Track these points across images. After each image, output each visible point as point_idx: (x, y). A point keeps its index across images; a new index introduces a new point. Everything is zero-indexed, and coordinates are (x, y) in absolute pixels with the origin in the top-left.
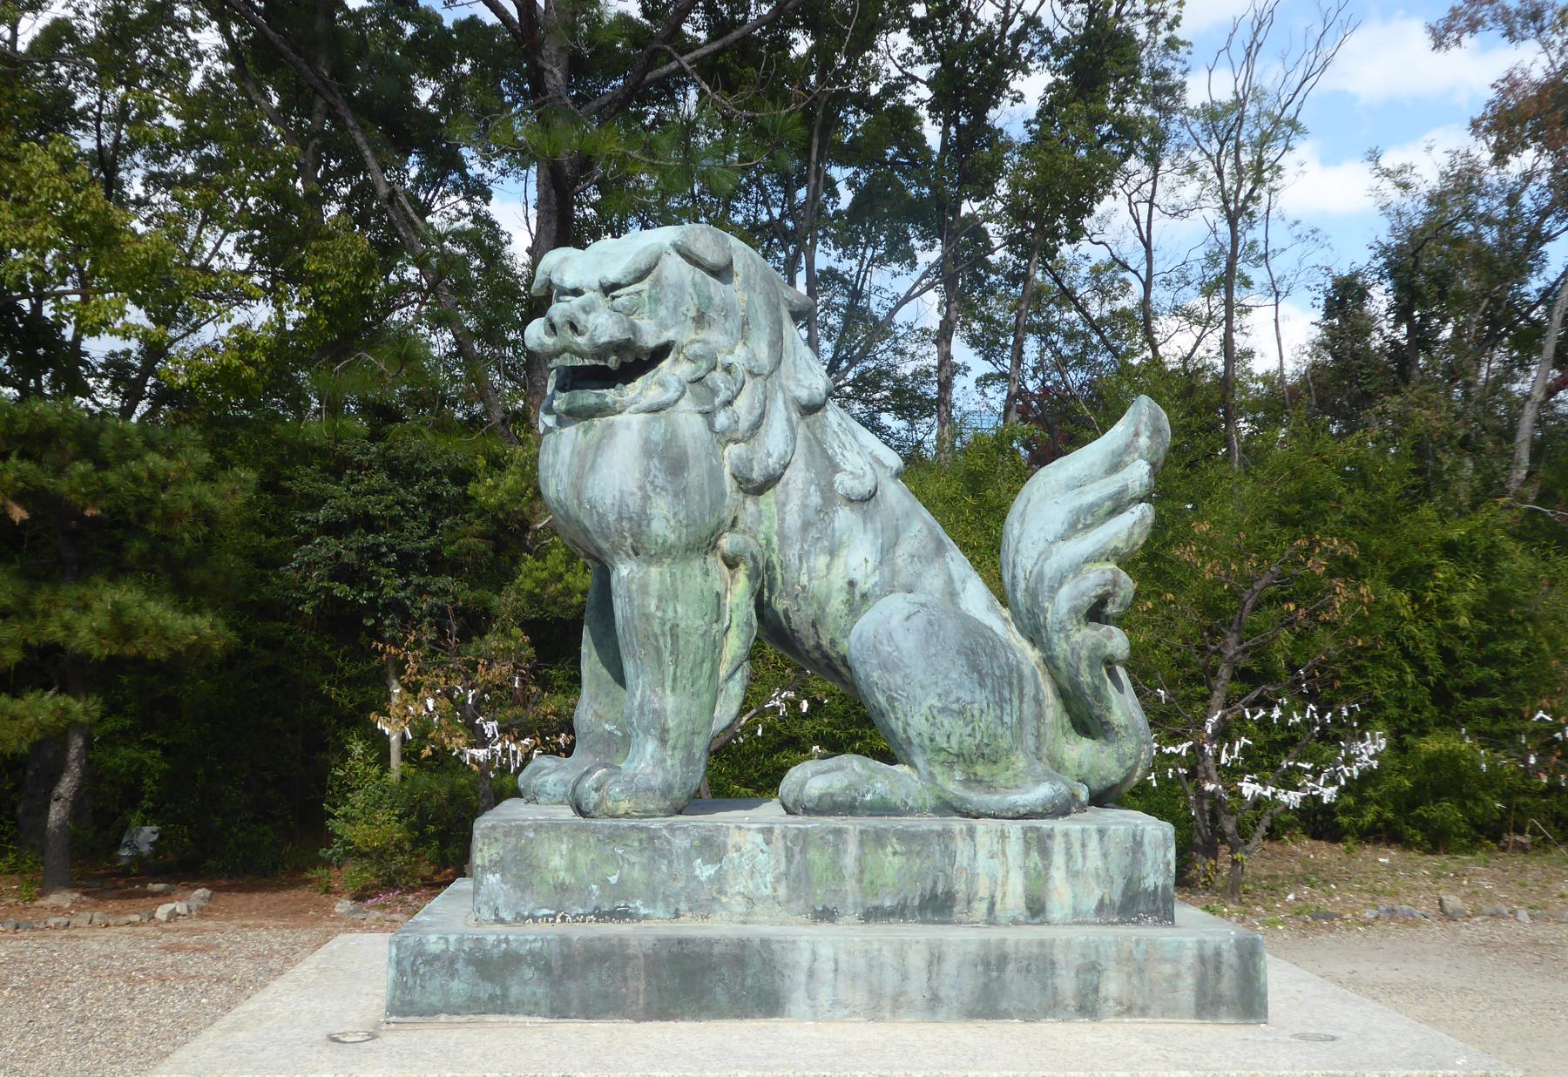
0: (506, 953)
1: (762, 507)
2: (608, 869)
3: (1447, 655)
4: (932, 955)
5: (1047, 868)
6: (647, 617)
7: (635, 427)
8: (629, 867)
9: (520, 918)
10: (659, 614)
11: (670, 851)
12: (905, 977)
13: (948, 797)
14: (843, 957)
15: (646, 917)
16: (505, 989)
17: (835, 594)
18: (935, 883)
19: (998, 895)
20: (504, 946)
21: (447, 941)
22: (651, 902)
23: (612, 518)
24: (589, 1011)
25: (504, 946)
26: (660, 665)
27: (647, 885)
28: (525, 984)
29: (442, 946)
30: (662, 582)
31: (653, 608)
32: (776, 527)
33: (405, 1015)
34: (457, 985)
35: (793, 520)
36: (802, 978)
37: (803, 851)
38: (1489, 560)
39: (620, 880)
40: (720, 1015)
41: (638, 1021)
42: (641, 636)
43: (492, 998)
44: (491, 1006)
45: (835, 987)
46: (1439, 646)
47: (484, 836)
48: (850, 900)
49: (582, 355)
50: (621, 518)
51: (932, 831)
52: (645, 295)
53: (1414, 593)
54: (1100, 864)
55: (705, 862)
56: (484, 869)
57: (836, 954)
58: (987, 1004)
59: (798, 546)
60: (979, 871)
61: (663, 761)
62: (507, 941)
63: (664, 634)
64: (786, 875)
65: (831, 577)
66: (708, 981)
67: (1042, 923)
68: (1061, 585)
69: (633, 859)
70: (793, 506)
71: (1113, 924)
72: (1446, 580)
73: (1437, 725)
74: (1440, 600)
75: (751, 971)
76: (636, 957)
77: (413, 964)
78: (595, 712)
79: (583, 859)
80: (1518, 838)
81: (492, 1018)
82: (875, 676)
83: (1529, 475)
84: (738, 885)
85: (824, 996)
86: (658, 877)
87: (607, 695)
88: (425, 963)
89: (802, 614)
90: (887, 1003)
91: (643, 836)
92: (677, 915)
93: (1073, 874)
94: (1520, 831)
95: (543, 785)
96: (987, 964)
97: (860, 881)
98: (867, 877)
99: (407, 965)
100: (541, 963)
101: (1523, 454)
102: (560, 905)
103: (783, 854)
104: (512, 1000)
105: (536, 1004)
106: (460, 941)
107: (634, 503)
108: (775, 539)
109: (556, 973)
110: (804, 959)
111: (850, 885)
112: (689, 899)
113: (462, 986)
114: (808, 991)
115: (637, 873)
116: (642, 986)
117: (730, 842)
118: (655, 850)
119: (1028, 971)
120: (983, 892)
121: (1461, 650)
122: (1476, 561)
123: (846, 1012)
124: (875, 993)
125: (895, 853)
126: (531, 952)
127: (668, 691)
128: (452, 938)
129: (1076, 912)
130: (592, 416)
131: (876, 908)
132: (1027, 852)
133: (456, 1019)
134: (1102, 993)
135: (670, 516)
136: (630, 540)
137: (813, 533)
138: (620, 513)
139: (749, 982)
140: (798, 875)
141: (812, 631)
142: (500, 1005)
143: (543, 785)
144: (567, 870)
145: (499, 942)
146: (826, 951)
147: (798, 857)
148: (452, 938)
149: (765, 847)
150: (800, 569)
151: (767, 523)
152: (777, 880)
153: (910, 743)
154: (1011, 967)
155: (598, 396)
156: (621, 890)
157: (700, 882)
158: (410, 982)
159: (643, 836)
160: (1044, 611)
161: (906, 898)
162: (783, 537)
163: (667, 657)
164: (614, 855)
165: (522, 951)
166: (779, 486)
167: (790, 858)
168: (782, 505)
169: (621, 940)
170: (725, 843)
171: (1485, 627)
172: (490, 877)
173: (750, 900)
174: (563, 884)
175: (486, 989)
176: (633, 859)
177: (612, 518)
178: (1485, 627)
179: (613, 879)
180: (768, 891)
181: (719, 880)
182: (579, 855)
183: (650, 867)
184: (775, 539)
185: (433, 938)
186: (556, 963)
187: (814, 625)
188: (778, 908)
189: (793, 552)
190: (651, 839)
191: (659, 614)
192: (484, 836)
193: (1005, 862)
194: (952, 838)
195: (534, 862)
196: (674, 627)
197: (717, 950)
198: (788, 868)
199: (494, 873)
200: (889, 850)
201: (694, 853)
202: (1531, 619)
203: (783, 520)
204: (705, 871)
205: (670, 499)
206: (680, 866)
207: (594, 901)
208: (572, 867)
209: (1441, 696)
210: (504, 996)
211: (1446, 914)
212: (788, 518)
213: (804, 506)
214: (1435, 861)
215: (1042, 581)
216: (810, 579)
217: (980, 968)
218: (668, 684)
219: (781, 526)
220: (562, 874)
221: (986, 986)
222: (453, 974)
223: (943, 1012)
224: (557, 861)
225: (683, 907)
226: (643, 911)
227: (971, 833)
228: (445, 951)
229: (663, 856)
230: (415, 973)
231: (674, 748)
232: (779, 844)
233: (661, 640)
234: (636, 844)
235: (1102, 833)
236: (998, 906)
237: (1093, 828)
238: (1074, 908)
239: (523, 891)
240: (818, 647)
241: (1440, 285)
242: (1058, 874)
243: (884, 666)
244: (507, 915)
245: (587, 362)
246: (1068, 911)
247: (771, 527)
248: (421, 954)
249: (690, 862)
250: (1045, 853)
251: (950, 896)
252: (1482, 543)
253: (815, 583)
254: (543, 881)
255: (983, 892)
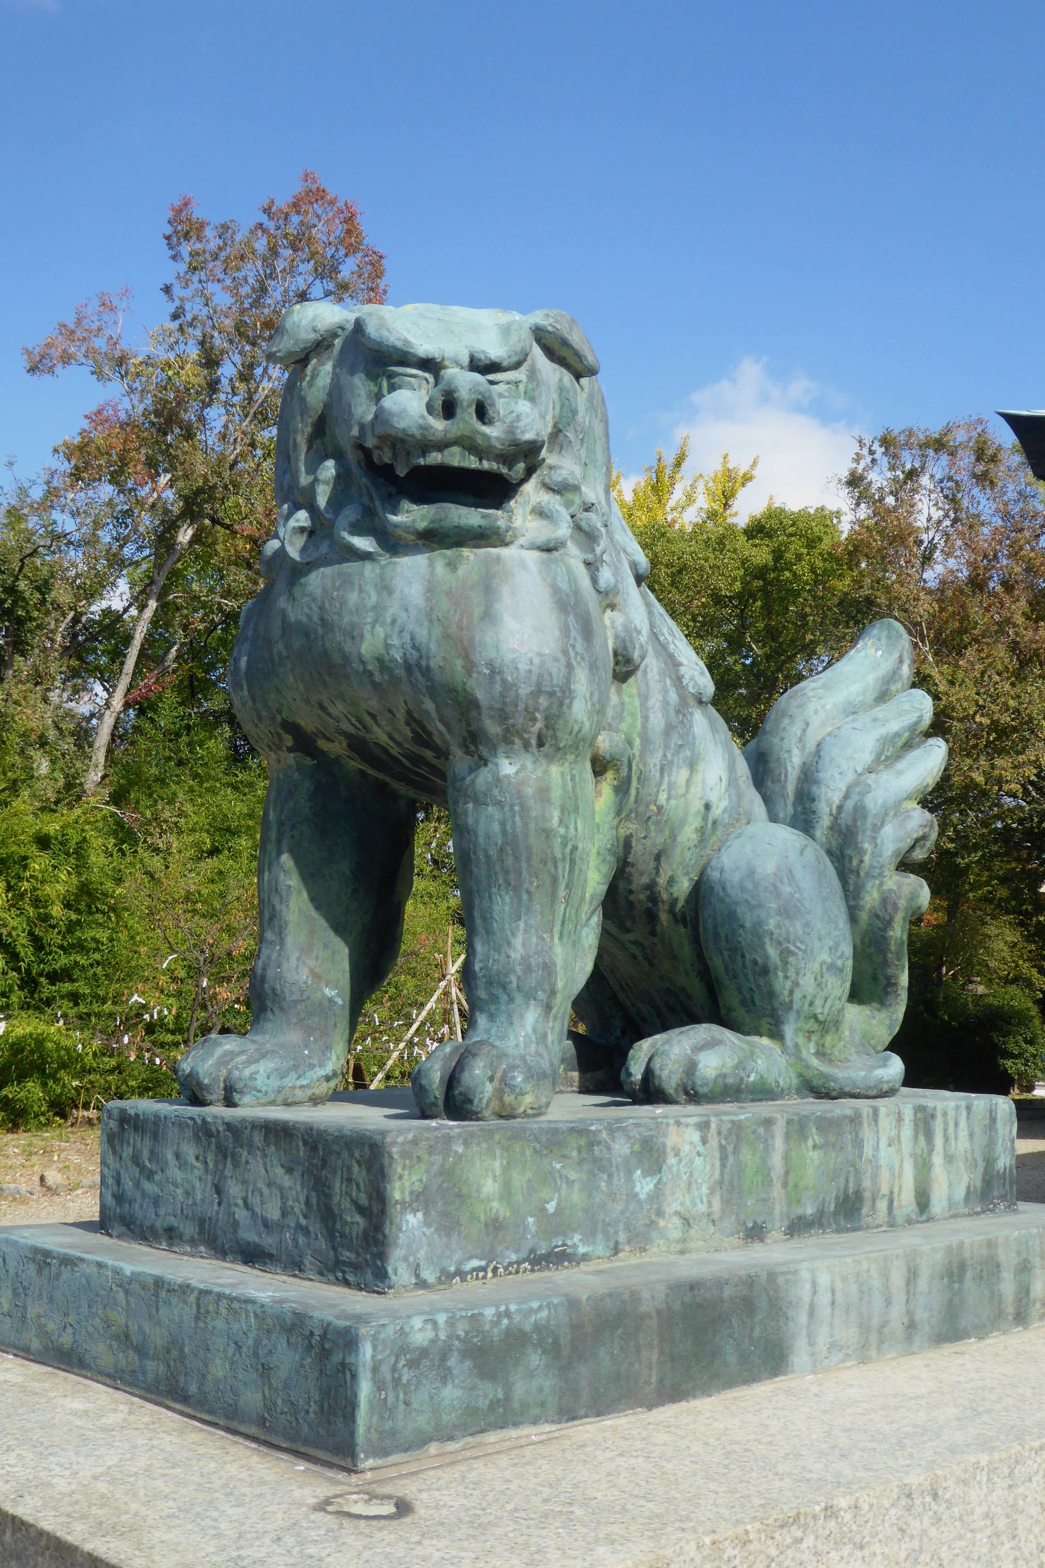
0: (508, 1333)
1: (626, 699)
2: (545, 1193)
3: (38, 943)
4: (909, 1270)
5: (931, 1151)
6: (547, 834)
7: (533, 567)
8: (567, 1191)
9: (446, 1277)
10: (562, 831)
11: (610, 1160)
12: (888, 1302)
13: (809, 1074)
14: (839, 1285)
15: (585, 1258)
16: (508, 1387)
17: (690, 819)
18: (847, 1181)
19: (896, 1190)
20: (505, 1321)
21: (435, 1323)
22: (589, 1236)
23: (524, 691)
24: (600, 1408)
25: (505, 1321)
26: (553, 902)
27: (586, 1211)
28: (533, 1377)
29: (430, 1334)
30: (564, 786)
31: (555, 821)
32: (639, 724)
33: (386, 1453)
34: (451, 1394)
35: (657, 721)
36: (803, 1318)
37: (736, 1150)
38: (80, 853)
39: (559, 1209)
40: (730, 1383)
41: (650, 1408)
42: (536, 859)
43: (493, 1405)
44: (491, 1419)
45: (831, 1325)
46: (31, 933)
47: (405, 1155)
48: (777, 1212)
49: (480, 453)
50: (538, 692)
51: (845, 1117)
52: (522, 387)
53: (8, 883)
54: (967, 1145)
55: (646, 1173)
56: (406, 1206)
57: (833, 1282)
58: (951, 1329)
59: (659, 754)
60: (882, 1162)
61: (544, 1036)
62: (507, 1314)
63: (564, 859)
64: (721, 1183)
65: (689, 796)
66: (713, 1338)
67: (928, 1221)
68: (883, 824)
69: (573, 1175)
70: (655, 701)
71: (977, 1214)
72: (41, 871)
73: (22, 1008)
74: (35, 889)
75: (759, 1317)
76: (649, 1316)
77: (394, 1369)
78: (311, 971)
79: (519, 1180)
80: (86, 1113)
81: (492, 1437)
82: (772, 923)
83: (103, 777)
84: (674, 1204)
85: (823, 1340)
86: (598, 1198)
87: (326, 947)
88: (412, 1364)
89: (648, 843)
90: (874, 1337)
91: (582, 1142)
92: (616, 1251)
93: (949, 1159)
94: (86, 1106)
95: (252, 1077)
96: (950, 1274)
97: (785, 1185)
98: (792, 1179)
99: (385, 1369)
100: (546, 1339)
101: (100, 756)
102: (492, 1250)
103: (717, 1155)
104: (516, 1405)
105: (543, 1405)
106: (451, 1322)
107: (557, 670)
108: (637, 742)
109: (565, 1353)
110: (804, 1293)
111: (777, 1191)
112: (628, 1229)
113: (459, 1393)
114: (809, 1336)
115: (577, 1197)
116: (655, 1356)
117: (669, 1143)
118: (595, 1160)
119: (981, 1278)
120: (885, 1190)
121: (53, 938)
122: (68, 854)
123: (840, 1356)
124: (864, 1328)
125: (815, 1147)
126: (537, 1328)
127: (556, 940)
128: (441, 1318)
129: (951, 1204)
130: (460, 544)
131: (800, 1218)
132: (916, 1138)
133: (451, 1446)
134: (1032, 1296)
135: (588, 695)
136: (539, 725)
137: (675, 740)
138: (539, 684)
139: (757, 1333)
140: (731, 1183)
141: (653, 864)
142: (503, 1415)
143: (252, 1077)
144: (501, 1199)
145: (499, 1315)
146: (824, 1279)
147: (731, 1158)
148: (441, 1318)
149: (700, 1148)
150: (660, 783)
151: (629, 720)
152: (712, 1192)
153: (789, 1007)
154: (969, 1275)
155: (484, 516)
156: (556, 1224)
157: (639, 1202)
158: (391, 1399)
159: (582, 1142)
160: (861, 852)
161: (824, 1202)
162: (646, 740)
163: (562, 892)
164: (552, 1172)
165: (528, 1328)
166: (639, 673)
167: (724, 1159)
168: (645, 698)
169: (633, 1293)
170: (664, 1145)
171: (74, 917)
172: (410, 1217)
173: (687, 1222)
174: (496, 1219)
175: (489, 1391)
176: (573, 1175)
177: (524, 691)
178: (74, 917)
179: (551, 1207)
180: (702, 1208)
181: (657, 1195)
182: (515, 1175)
183: (590, 1187)
184: (637, 742)
185: (417, 1322)
186: (565, 1340)
187: (658, 858)
188: (712, 1229)
189: (655, 760)
190: (591, 1145)
191: (562, 831)
192: (405, 1155)
193: (899, 1151)
194: (861, 1123)
195: (464, 1191)
196: (575, 848)
197: (727, 1293)
198: (722, 1174)
199: (415, 1211)
200: (810, 1143)
201: (634, 1161)
202: (113, 909)
203: (646, 718)
204: (644, 1186)
205: (587, 671)
206: (619, 1180)
207: (530, 1242)
208: (506, 1194)
209: (29, 983)
210: (508, 1399)
211: (49, 1189)
212: (652, 717)
213: (666, 703)
214: (21, 1139)
215: (865, 817)
216: (668, 799)
217: (946, 1280)
218: (557, 928)
219: (644, 726)
220: (495, 1204)
221: (951, 1300)
222: (445, 1376)
223: (917, 1338)
224: (490, 1187)
225: (622, 1237)
226: (582, 1250)
227: (876, 1111)
228: (434, 1341)
229: (602, 1169)
230: (397, 1382)
231: (555, 1019)
232: (714, 1142)
233: (560, 865)
234: (575, 1154)
235: (968, 1108)
236: (895, 1204)
237: (963, 1104)
238: (949, 1200)
239: (449, 1235)
240: (651, 886)
241: (43, 594)
242: (938, 1160)
243: (785, 912)
244: (429, 1275)
245: (486, 465)
246: (945, 1203)
247: (633, 726)
248: (402, 1350)
249: (630, 1173)
250: (929, 1136)
251: (859, 1196)
252: (74, 838)
253: (673, 802)
254: (473, 1218)
255: (885, 1190)
